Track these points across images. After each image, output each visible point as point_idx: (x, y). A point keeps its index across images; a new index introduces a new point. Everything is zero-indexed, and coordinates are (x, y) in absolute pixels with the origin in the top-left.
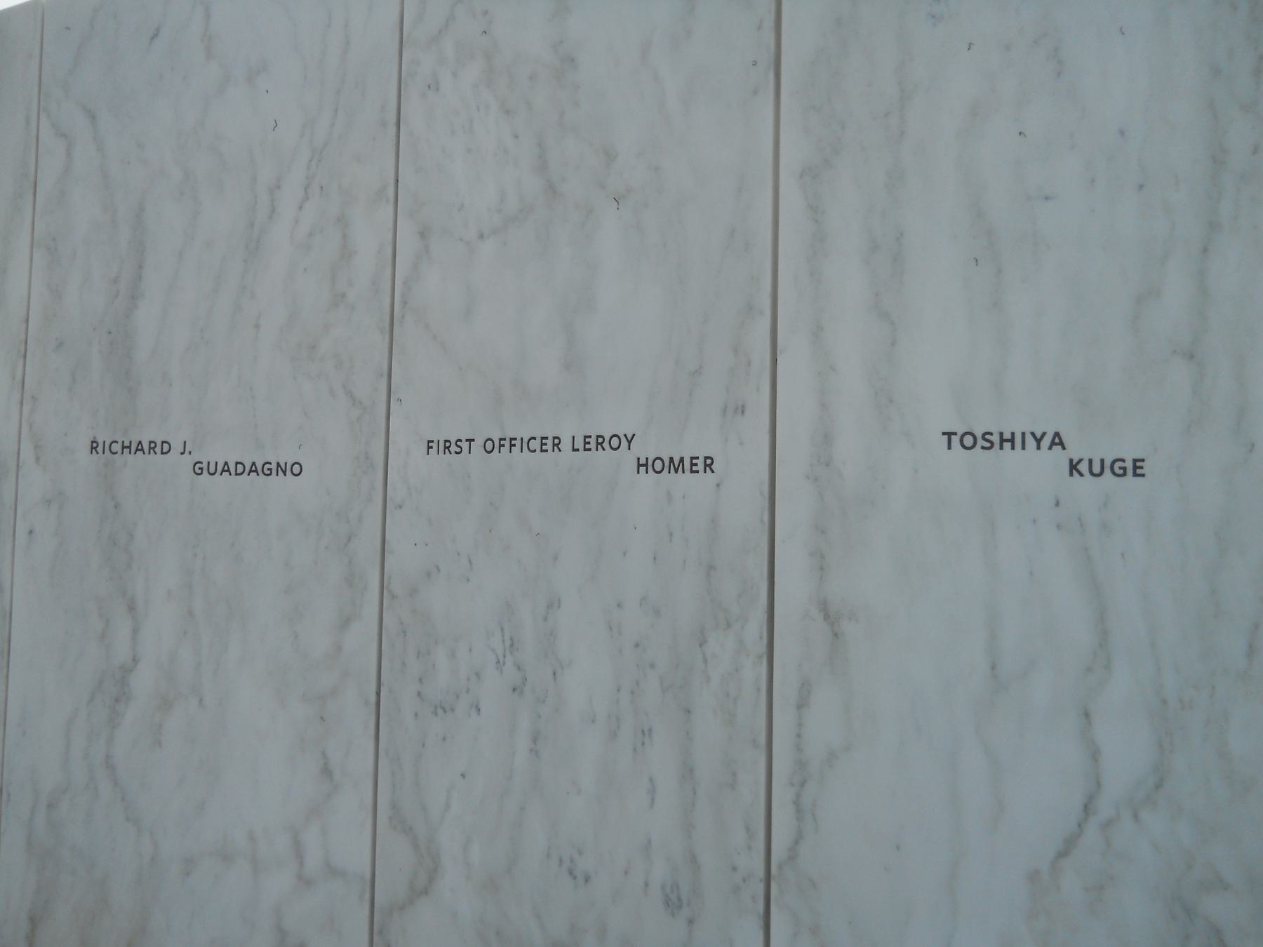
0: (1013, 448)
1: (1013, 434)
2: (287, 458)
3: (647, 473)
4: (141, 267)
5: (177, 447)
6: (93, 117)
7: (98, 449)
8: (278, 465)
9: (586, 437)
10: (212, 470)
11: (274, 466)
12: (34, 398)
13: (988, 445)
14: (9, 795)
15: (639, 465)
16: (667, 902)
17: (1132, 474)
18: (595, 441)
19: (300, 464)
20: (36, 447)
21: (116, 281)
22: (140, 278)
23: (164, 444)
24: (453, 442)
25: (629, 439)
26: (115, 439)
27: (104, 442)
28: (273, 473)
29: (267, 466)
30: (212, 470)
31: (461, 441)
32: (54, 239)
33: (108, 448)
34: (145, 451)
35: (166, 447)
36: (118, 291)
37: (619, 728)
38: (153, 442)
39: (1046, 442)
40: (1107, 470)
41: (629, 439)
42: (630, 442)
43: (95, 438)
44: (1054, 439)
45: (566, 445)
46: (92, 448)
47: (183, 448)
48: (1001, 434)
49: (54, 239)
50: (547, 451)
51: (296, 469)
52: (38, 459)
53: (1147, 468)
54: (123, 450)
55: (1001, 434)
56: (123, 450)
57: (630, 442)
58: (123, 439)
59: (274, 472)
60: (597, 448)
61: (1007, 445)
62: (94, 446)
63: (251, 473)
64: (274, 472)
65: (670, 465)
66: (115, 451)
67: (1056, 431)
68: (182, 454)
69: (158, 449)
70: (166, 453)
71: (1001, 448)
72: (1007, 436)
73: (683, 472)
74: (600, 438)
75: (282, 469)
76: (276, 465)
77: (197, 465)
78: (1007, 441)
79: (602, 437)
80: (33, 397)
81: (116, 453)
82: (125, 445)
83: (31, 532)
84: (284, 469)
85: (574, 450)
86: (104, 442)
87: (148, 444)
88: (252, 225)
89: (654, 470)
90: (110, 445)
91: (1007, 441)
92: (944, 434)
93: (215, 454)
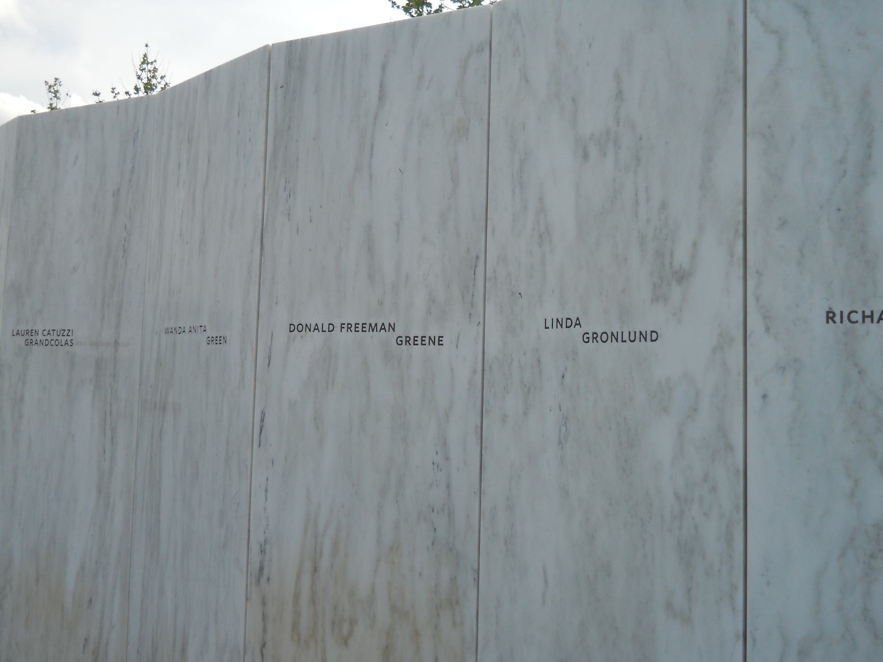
1: (872, 312)
4: (869, 147)
5: (187, 330)
6: (805, 12)
7: (351, 329)
9: (342, 324)
10: (632, 338)
12: (759, 274)
14: (754, 640)
16: (265, 552)
18: (347, 327)
19: (657, 334)
20: (765, 318)
21: (842, 160)
22: (870, 156)
28: (590, 341)
29: (586, 336)
30: (632, 338)
32: (769, 127)
35: (654, 335)
36: (845, 171)
40: (50, 341)
43: (830, 308)
49: (769, 127)
50: (358, 331)
52: (768, 329)
53: (445, 341)
54: (341, 330)
55: (863, 312)
56: (341, 330)
58: (864, 309)
59: (591, 340)
61: (868, 320)
62: (830, 316)
69: (353, 329)
70: (654, 341)
73: (842, 313)
75: (432, 341)
76: (611, 334)
77: (585, 335)
80: (757, 272)
81: (857, 322)
83: (764, 396)
85: (546, 328)
87: (354, 324)
89: (302, 326)
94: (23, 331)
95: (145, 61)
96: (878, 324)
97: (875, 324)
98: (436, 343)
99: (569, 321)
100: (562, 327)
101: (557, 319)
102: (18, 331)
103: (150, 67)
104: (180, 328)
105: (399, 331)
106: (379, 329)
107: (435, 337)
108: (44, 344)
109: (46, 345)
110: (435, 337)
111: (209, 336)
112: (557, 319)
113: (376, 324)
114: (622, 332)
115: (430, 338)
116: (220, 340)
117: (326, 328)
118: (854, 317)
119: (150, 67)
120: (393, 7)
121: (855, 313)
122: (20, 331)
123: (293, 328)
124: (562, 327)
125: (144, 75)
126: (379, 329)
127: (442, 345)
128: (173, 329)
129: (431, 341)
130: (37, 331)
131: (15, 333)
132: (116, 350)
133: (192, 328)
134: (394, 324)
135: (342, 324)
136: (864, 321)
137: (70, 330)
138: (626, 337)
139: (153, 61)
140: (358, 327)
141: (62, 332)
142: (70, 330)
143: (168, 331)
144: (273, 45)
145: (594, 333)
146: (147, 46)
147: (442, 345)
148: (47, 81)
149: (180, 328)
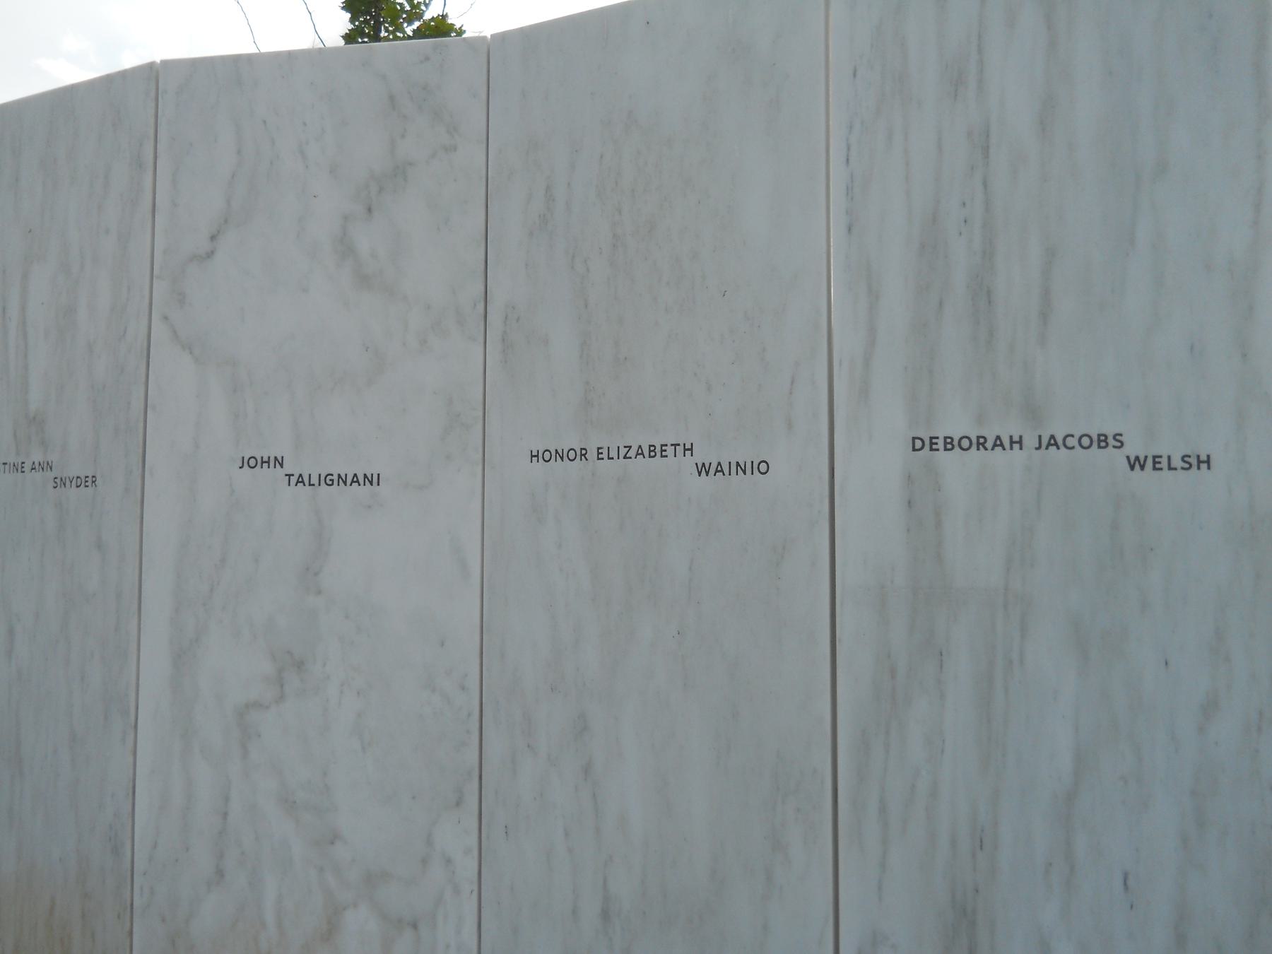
2: (745, 455)
3: (737, 474)
8: (339, 476)
9: (599, 449)
11: (335, 478)
13: (1187, 466)
15: (691, 450)
23: (916, 441)
25: (628, 449)
26: (79, 488)
29: (329, 477)
33: (926, 443)
34: (1059, 444)
37: (588, 270)
38: (949, 438)
39: (294, 480)
41: (628, 449)
44: (996, 441)
45: (27, 467)
47: (241, 462)
48: (1011, 437)
50: (603, 459)
51: (763, 467)
57: (71, 482)
59: (336, 482)
60: (275, 465)
63: (717, 474)
64: (336, 482)
65: (365, 481)
66: (1072, 446)
68: (1037, 449)
72: (265, 459)
74: (652, 448)
75: (369, 480)
76: (554, 451)
82: (264, 460)
84: (366, 480)
90: (248, 461)
92: (286, 475)
93: (311, 469)
97: (989, 452)
102: (34, 463)
107: (372, 475)
110: (372, 475)
114: (310, 475)
118: (1070, 442)
121: (1071, 438)
122: (37, 464)
123: (917, 444)
127: (666, 456)
129: (366, 480)
130: (50, 463)
131: (1045, 441)
132: (949, 443)
135: (599, 449)
136: (1011, 448)
137: (625, 457)
138: (613, 454)
139: (1110, 432)
141: (623, 451)
142: (625, 457)
147: (666, 456)
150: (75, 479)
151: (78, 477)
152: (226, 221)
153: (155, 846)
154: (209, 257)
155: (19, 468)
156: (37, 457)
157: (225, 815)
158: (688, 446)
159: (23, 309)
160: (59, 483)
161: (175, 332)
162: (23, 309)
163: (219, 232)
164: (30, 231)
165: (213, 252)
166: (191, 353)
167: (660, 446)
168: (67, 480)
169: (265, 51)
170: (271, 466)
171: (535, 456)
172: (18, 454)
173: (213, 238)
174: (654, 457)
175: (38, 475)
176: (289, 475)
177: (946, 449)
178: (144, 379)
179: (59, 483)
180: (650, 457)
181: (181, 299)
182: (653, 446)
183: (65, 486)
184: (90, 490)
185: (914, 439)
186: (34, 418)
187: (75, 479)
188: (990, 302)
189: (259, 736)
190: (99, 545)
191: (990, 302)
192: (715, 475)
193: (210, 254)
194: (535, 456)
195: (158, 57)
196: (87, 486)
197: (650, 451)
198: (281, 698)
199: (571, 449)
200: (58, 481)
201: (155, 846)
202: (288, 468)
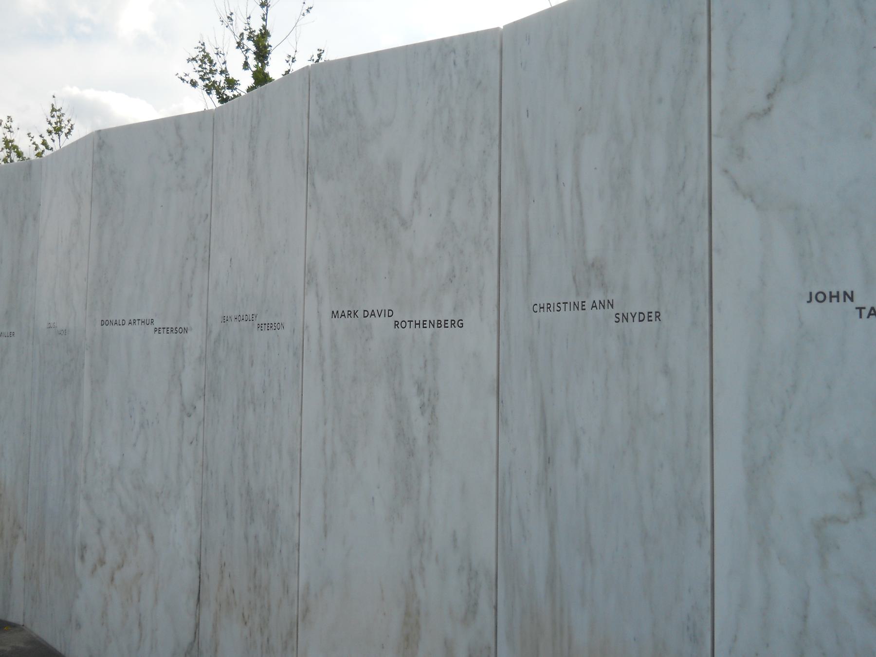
0: (838, 301)
1: (838, 293)
5: (127, 323)
17: (647, 320)
23: (641, 314)
24: (178, 332)
27: (613, 300)
29: (460, 322)
31: (560, 303)
33: (827, 296)
35: (390, 313)
39: (865, 313)
42: (633, 317)
45: (588, 305)
46: (395, 325)
57: (633, 317)
67: (873, 306)
68: (808, 302)
70: (366, 317)
71: (831, 301)
72: (834, 293)
76: (599, 302)
78: (834, 297)
79: (549, 304)
84: (433, 324)
86: (554, 304)
88: (197, 440)
91: (834, 297)
92: (857, 308)
94: (148, 321)
95: (53, 110)
96: (810, 291)
98: (421, 325)
99: (390, 312)
100: (604, 308)
101: (574, 303)
102: (130, 320)
103: (58, 113)
104: (246, 315)
105: (151, 328)
106: (339, 316)
107: (434, 321)
108: (281, 324)
109: (107, 325)
110: (434, 321)
111: (241, 32)
112: (333, 312)
113: (337, 312)
115: (430, 321)
116: (262, 327)
117: (121, 323)
119: (58, 113)
120: (237, 47)
123: (334, 314)
124: (604, 308)
125: (53, 120)
126: (339, 316)
127: (585, 309)
128: (229, 317)
133: (229, 317)
134: (613, 300)
140: (651, 316)
143: (12, 334)
144: (504, 27)
145: (452, 321)
146: (54, 97)
147: (585, 309)
148: (9, 116)
149: (246, 315)
150: (637, 315)
151: (640, 313)
152: (782, 80)
153: (735, 639)
154: (765, 113)
155: (579, 306)
156: (598, 296)
157: (805, 618)
158: (417, 322)
159: (577, 174)
160: (621, 319)
161: (735, 183)
162: (577, 174)
163: (775, 90)
164: (580, 109)
165: (769, 109)
166: (752, 201)
167: (444, 321)
168: (630, 315)
169: (555, 5)
170: (840, 300)
171: (418, 324)
172: (578, 294)
173: (769, 96)
174: (440, 327)
175: (600, 312)
176: (861, 309)
177: (389, 316)
178: (706, 225)
179: (621, 319)
180: (438, 327)
181: (741, 153)
182: (440, 321)
183: (574, 303)
184: (655, 324)
185: (364, 311)
186: (593, 265)
187: (637, 315)
188: (181, 284)
189: (838, 548)
190: (666, 371)
191: (181, 284)
192: (592, 309)
193: (768, 111)
194: (418, 324)
195: (350, 56)
196: (168, 333)
197: (438, 324)
198: (860, 514)
199: (403, 321)
200: (620, 316)
201: (735, 639)
202: (859, 301)
